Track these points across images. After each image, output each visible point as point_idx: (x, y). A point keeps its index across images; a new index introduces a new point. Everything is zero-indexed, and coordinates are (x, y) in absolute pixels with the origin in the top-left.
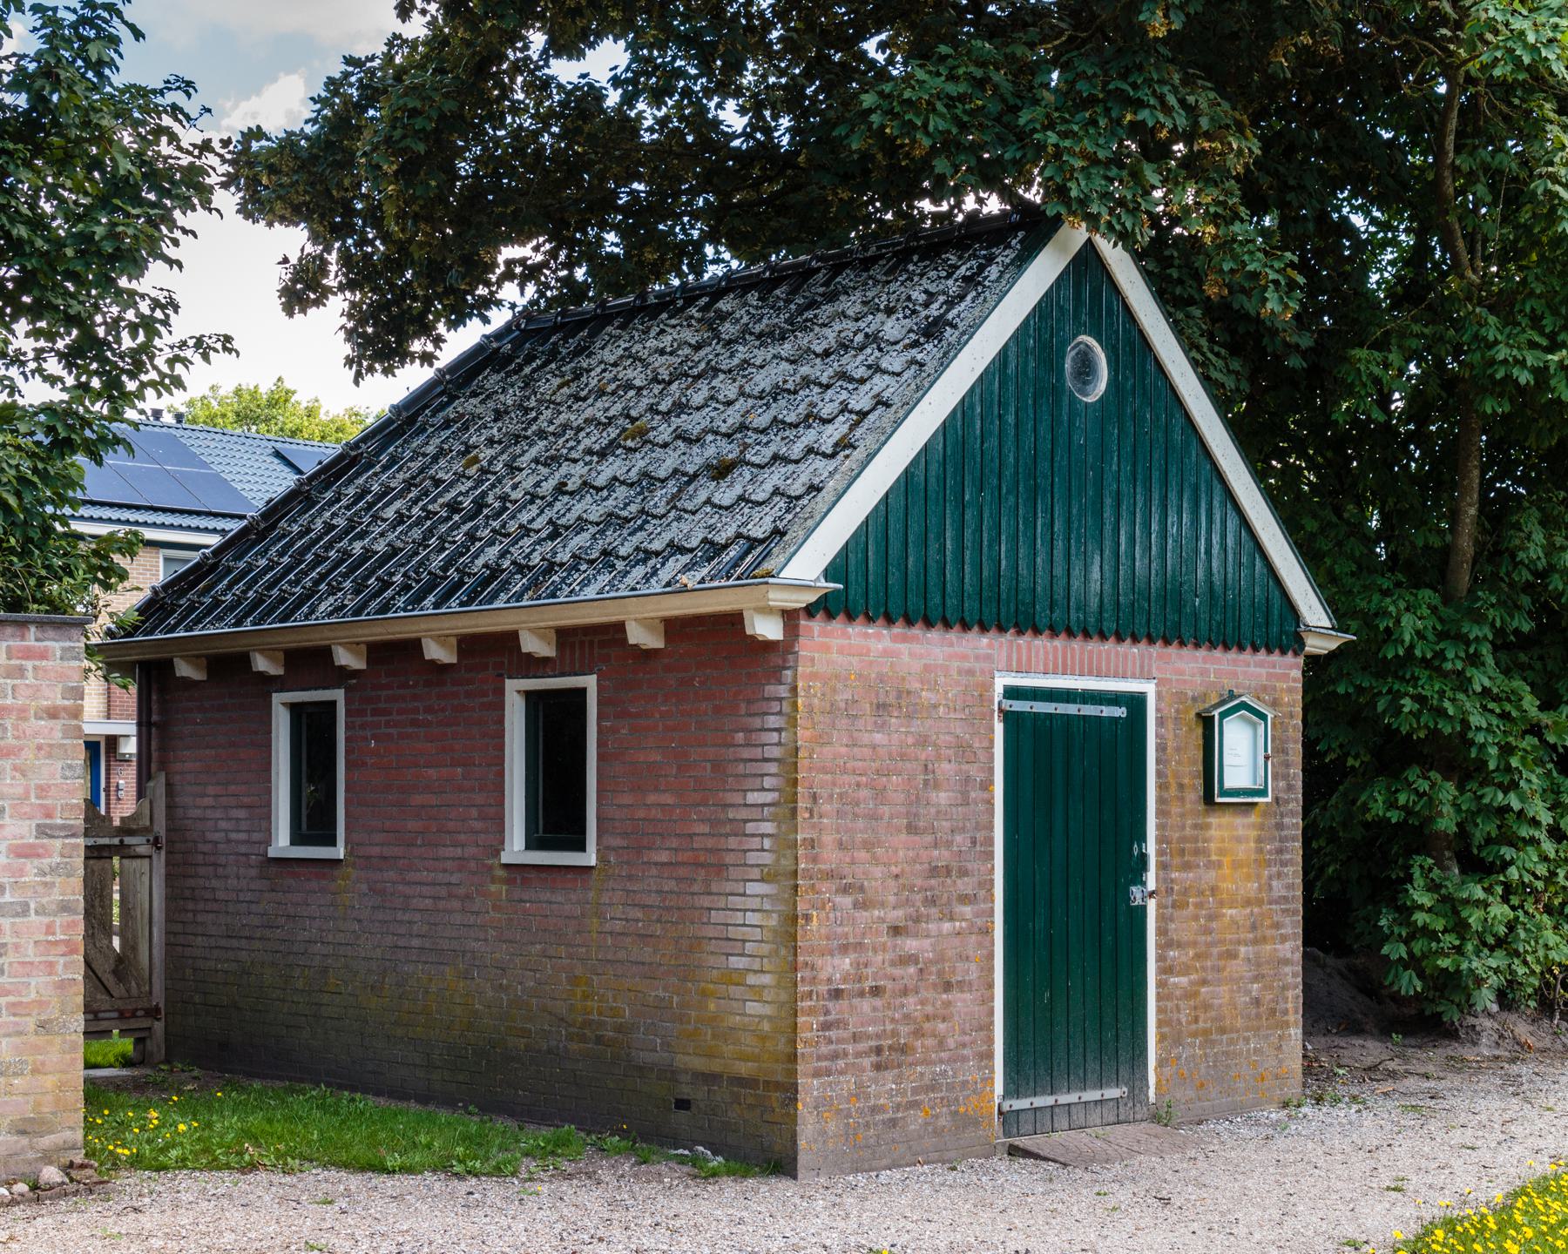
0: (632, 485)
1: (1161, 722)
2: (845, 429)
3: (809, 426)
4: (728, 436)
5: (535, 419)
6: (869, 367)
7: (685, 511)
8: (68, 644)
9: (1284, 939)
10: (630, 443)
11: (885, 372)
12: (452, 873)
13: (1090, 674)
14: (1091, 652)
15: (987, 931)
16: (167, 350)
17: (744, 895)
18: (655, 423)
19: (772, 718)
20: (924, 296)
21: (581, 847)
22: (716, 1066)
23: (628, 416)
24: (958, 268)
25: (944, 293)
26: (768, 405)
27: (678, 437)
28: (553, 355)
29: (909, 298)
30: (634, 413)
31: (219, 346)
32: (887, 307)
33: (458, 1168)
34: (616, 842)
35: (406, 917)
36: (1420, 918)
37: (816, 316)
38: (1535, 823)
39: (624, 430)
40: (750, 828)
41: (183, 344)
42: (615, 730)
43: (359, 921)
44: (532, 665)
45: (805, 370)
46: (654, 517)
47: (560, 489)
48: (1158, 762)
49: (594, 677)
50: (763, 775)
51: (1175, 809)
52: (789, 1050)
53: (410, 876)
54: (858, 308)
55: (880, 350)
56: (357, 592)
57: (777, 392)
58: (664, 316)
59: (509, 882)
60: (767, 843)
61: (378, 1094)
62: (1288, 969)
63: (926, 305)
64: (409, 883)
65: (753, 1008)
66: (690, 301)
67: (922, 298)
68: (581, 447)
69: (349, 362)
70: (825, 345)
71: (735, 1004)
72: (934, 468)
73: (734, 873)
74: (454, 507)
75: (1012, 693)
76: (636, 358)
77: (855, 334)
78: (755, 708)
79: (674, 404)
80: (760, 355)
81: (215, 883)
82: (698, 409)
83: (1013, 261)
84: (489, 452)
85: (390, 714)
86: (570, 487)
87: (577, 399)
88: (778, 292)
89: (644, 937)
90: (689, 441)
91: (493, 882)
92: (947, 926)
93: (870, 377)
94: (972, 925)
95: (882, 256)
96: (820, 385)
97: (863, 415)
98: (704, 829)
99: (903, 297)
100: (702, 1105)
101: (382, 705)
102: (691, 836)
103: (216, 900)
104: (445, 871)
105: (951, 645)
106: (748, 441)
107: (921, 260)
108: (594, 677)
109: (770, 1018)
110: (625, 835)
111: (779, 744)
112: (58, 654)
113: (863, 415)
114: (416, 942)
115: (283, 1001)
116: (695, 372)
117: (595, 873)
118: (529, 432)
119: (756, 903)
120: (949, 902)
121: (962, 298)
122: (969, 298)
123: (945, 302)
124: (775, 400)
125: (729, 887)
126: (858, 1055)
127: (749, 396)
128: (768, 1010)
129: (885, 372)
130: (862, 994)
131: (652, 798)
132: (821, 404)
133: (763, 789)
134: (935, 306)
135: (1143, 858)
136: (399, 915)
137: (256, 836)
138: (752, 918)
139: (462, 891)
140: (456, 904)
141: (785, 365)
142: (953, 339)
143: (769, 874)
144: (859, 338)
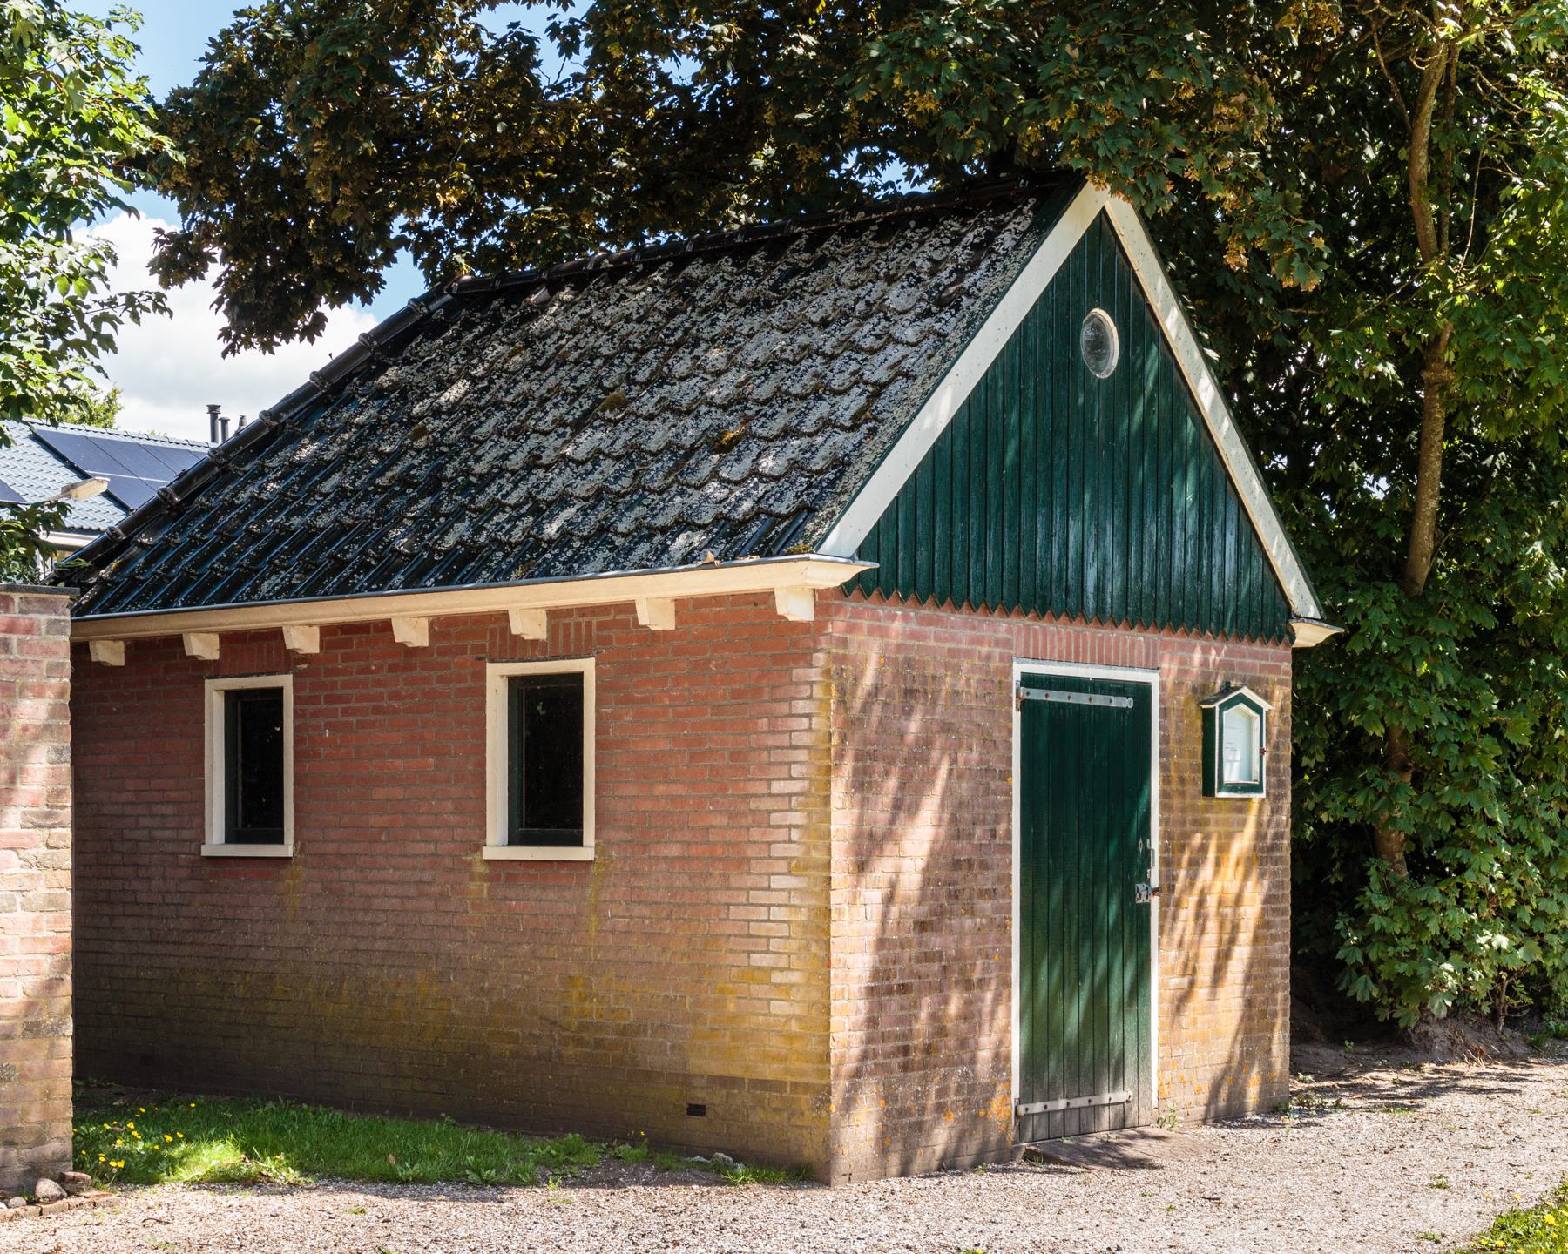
0: (618, 458)
1: (1164, 713)
2: (862, 401)
3: (820, 398)
4: (724, 408)
5: (487, 389)
6: (878, 337)
7: (689, 485)
8: (53, 617)
9: (1274, 938)
10: (608, 414)
11: (897, 342)
12: (423, 870)
13: (1100, 663)
14: (1101, 639)
15: (1004, 927)
16: (97, 307)
17: (769, 889)
18: (633, 394)
19: (801, 703)
20: (929, 264)
21: (577, 841)
22: (735, 1071)
23: (600, 386)
24: (964, 235)
25: (953, 261)
26: (766, 375)
27: (665, 409)
28: (496, 321)
29: (913, 265)
30: (606, 383)
31: (149, 304)
32: (887, 274)
33: (473, 1177)
34: (620, 835)
35: (369, 918)
36: (1377, 922)
37: (805, 283)
38: (1491, 823)
39: (598, 401)
40: (775, 818)
41: (112, 302)
42: (615, 717)
43: (311, 923)
44: (516, 648)
45: (803, 339)
46: (652, 491)
47: (533, 463)
48: (1162, 755)
49: (593, 660)
50: (790, 764)
51: (1176, 802)
52: (820, 1049)
53: (371, 875)
54: (853, 275)
55: (887, 319)
56: (306, 571)
57: (773, 363)
58: (624, 280)
59: (490, 878)
60: (795, 835)
61: (338, 1106)
62: (1278, 970)
63: (933, 273)
64: (371, 883)
65: (778, 1007)
66: (651, 267)
67: (927, 265)
68: (549, 418)
69: (225, 333)
70: (821, 313)
71: (757, 1004)
72: (959, 442)
73: (756, 867)
74: (405, 480)
75: (1029, 681)
76: (597, 325)
77: (856, 302)
78: (779, 694)
79: (652, 374)
80: (746, 325)
81: (135, 885)
82: (683, 379)
83: (1030, 229)
84: (437, 424)
85: (348, 700)
86: (545, 460)
87: (534, 368)
88: (756, 258)
89: (650, 936)
90: (679, 414)
91: (472, 879)
92: (968, 922)
93: (882, 348)
94: (992, 920)
95: (872, 222)
96: (824, 355)
97: (880, 388)
98: (721, 820)
99: (904, 264)
100: (719, 1110)
101: (340, 692)
102: (707, 829)
103: (137, 904)
104: (414, 868)
105: (973, 628)
106: (749, 413)
107: (918, 226)
108: (593, 660)
109: (799, 1018)
110: (629, 829)
111: (810, 730)
112: (44, 628)
113: (880, 388)
114: (380, 945)
115: (220, 1009)
116: (672, 340)
117: (593, 869)
118: (483, 403)
119: (782, 898)
120: (971, 897)
121: (974, 266)
122: (983, 266)
123: (955, 270)
124: (773, 370)
125: (750, 881)
126: (888, 1055)
127: (742, 366)
128: (796, 1010)
129: (897, 342)
130: (890, 992)
131: (660, 789)
132: (830, 375)
133: (791, 778)
134: (945, 274)
135: (1147, 853)
136: (360, 916)
137: (186, 834)
138: (777, 913)
139: (435, 889)
140: (429, 904)
141: (776, 334)
142: (976, 308)
143: (797, 867)
144: (861, 306)
